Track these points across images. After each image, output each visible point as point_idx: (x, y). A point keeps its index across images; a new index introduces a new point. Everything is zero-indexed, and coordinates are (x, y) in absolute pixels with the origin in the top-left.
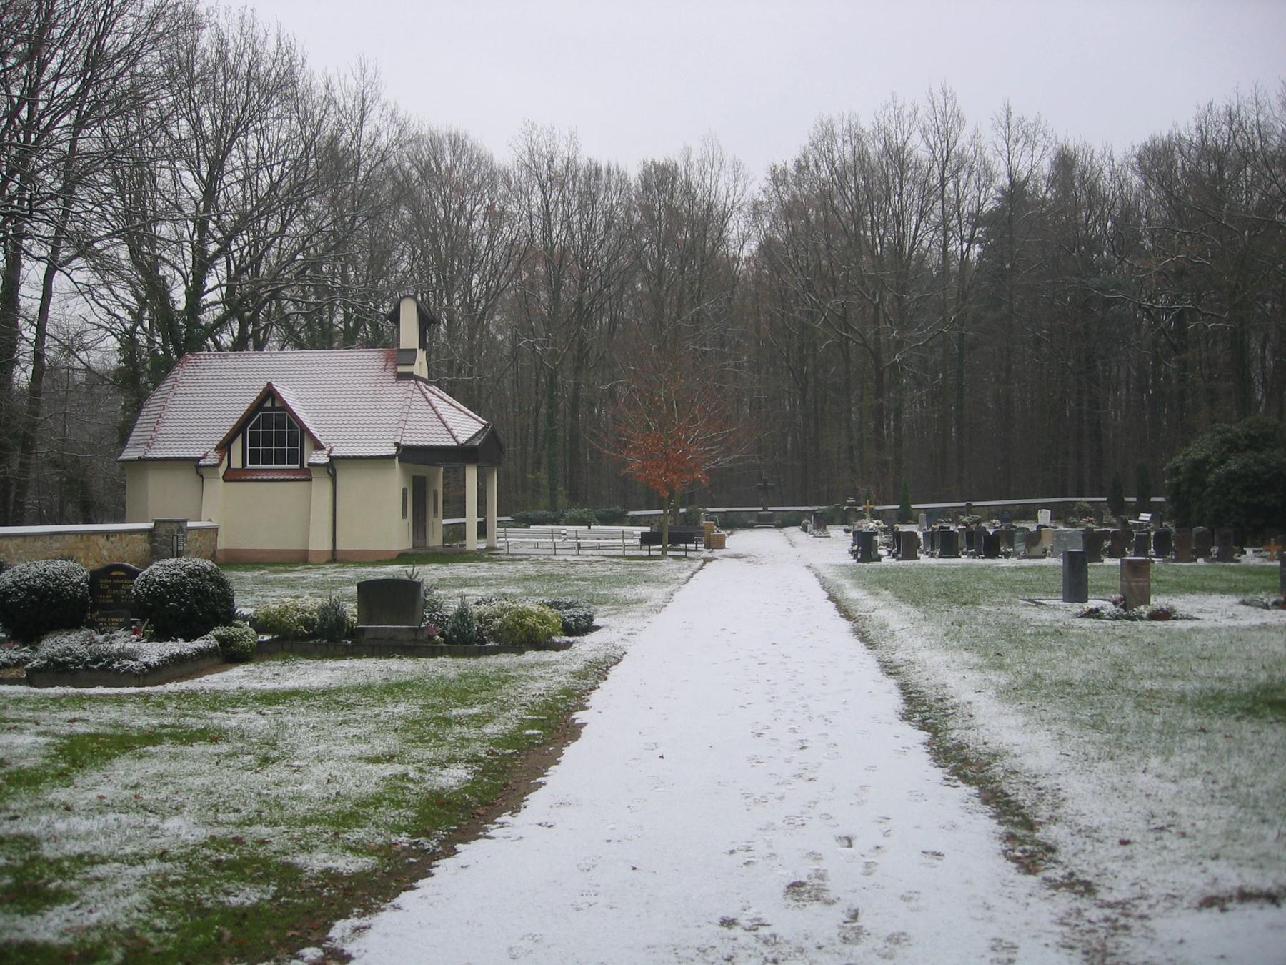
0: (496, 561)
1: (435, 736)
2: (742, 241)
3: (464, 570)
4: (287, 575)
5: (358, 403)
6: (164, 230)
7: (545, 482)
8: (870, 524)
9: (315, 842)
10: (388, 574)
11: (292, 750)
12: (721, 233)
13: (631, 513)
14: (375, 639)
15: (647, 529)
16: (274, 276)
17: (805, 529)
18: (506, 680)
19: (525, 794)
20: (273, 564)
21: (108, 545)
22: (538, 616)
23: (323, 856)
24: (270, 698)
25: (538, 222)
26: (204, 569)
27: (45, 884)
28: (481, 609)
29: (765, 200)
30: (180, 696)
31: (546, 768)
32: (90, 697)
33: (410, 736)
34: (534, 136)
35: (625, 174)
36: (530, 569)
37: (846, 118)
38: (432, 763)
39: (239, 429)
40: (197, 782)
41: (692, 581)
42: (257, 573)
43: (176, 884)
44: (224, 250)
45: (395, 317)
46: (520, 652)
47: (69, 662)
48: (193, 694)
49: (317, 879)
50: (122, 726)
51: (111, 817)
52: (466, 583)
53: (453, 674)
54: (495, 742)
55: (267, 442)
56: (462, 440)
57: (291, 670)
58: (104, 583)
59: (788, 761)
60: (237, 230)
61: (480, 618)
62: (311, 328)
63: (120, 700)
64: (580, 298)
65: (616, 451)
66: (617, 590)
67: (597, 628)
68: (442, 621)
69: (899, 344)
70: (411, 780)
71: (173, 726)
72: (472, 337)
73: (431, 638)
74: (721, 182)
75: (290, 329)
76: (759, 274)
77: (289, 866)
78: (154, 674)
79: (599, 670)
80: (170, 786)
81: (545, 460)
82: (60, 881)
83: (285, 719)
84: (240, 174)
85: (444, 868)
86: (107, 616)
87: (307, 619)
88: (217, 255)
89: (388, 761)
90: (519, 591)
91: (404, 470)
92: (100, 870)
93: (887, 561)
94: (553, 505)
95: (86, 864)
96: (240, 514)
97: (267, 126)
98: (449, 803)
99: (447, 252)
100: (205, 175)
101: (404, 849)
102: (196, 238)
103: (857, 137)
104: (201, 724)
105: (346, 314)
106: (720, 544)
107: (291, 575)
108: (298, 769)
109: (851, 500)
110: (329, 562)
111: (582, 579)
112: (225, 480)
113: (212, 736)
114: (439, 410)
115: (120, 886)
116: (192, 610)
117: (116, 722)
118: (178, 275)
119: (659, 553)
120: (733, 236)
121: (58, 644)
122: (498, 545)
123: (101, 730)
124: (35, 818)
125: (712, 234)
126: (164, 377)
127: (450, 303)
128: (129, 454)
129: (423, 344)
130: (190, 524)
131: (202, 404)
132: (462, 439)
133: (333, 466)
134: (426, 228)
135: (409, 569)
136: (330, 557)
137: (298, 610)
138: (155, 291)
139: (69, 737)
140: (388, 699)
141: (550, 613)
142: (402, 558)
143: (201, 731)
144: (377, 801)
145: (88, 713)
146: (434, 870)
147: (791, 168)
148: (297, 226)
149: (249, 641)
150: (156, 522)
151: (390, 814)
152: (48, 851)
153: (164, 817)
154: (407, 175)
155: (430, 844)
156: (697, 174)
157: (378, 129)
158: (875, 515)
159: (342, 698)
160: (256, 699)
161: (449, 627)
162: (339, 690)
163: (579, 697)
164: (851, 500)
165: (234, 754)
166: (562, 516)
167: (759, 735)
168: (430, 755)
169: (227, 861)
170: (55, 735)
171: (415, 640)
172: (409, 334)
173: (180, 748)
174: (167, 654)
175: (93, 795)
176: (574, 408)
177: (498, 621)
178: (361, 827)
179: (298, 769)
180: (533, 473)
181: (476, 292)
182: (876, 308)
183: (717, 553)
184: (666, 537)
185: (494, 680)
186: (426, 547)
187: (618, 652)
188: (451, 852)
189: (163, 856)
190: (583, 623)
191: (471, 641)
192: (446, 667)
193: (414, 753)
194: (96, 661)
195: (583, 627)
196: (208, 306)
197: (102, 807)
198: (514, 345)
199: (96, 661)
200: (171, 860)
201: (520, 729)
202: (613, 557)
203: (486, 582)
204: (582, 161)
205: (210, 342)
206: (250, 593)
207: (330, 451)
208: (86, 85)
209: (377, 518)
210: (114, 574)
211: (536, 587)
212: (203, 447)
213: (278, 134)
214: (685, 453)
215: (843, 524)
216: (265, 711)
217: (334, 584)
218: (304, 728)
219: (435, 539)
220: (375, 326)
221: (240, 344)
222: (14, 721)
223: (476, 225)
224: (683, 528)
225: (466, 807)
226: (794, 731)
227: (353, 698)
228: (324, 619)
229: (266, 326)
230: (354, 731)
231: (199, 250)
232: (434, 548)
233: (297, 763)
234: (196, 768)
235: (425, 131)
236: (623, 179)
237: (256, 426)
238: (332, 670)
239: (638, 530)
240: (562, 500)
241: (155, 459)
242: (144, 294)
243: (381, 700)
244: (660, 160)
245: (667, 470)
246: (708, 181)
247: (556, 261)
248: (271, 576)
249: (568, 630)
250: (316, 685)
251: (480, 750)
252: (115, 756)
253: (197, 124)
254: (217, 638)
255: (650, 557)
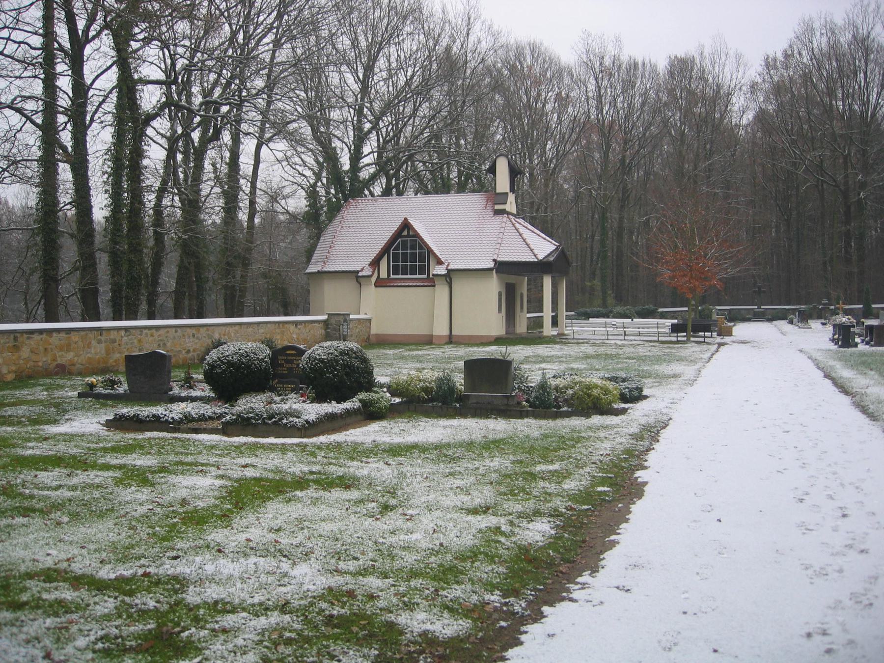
0: (565, 343)
1: (523, 490)
2: (743, 111)
3: (542, 350)
4: (417, 352)
5: (468, 231)
6: (335, 115)
7: (599, 288)
8: (844, 319)
9: (417, 599)
10: (489, 352)
11: (408, 499)
12: (727, 107)
13: (660, 310)
14: (477, 403)
15: (675, 321)
16: (409, 145)
17: (791, 322)
18: (579, 440)
19: (602, 552)
20: (408, 344)
21: (297, 331)
22: (601, 388)
23: (422, 616)
24: (395, 451)
25: (593, 103)
26: (352, 350)
27: (180, 632)
28: (558, 381)
29: (760, 81)
30: (328, 447)
31: (618, 524)
32: (263, 446)
33: (503, 489)
34: (590, 41)
35: (656, 66)
36: (590, 350)
37: (823, 16)
38: (520, 515)
39: (385, 250)
40: (327, 528)
41: (712, 360)
42: (397, 351)
43: (289, 642)
44: (375, 127)
45: (492, 170)
46: (588, 416)
47: (251, 418)
48: (338, 445)
49: (415, 643)
50: (280, 472)
51: (253, 559)
52: (544, 360)
53: (536, 434)
54: (572, 498)
55: (405, 259)
56: (541, 257)
57: (414, 427)
58: (281, 359)
59: (835, 529)
60: (383, 113)
61: (557, 388)
62: (435, 181)
63: (284, 449)
64: (624, 157)
65: (652, 265)
66: (656, 367)
67: (646, 397)
68: (528, 391)
69: (863, 185)
70: (503, 534)
71: (319, 473)
72: (546, 185)
73: (519, 403)
74: (727, 69)
75: (421, 182)
76: (754, 135)
77: (391, 625)
78: (312, 428)
79: (651, 433)
80: (306, 531)
81: (598, 272)
82: (193, 629)
83: (404, 470)
84: (384, 74)
85: (533, 633)
86: (283, 383)
87: (427, 387)
88: (370, 132)
89: (485, 512)
90: (583, 366)
91: (499, 278)
92: (229, 620)
93: (862, 347)
94: (604, 304)
95: (219, 612)
96: (386, 309)
97: (403, 40)
98: (535, 559)
99: (528, 128)
100: (361, 77)
101: (495, 608)
102: (355, 118)
103: (832, 30)
104: (340, 471)
105: (459, 170)
106: (729, 333)
107: (420, 353)
108: (411, 518)
109: (825, 301)
110: (447, 343)
111: (629, 358)
112: (376, 286)
113: (346, 483)
114: (524, 236)
115: (240, 642)
116: (342, 380)
117: (277, 468)
118: (344, 146)
119: (685, 339)
120: (735, 108)
121: (253, 403)
122: (566, 332)
123: (265, 474)
124: (191, 558)
125: (721, 104)
126: (335, 216)
127: (531, 161)
128: (312, 269)
129: (512, 190)
130: (351, 317)
131: (360, 234)
132: (541, 257)
133: (450, 276)
134: (514, 110)
135: (503, 349)
136: (447, 340)
137: (420, 381)
138: (331, 157)
139: (238, 480)
140: (486, 455)
141: (610, 385)
142: (498, 341)
143: (341, 478)
144: (473, 555)
145: (258, 460)
146: (523, 638)
147: (780, 57)
148: (425, 109)
149: (384, 403)
150: (329, 315)
151: (484, 570)
152: (192, 597)
153: (294, 564)
154: (499, 71)
155: (519, 606)
156: (708, 63)
157: (480, 40)
158: (846, 312)
159: (450, 453)
160: (384, 451)
161: (533, 395)
162: (448, 445)
163: (638, 457)
164: (825, 301)
165: (361, 501)
166: (611, 312)
167: (801, 500)
168: (519, 508)
169: (340, 616)
170: (230, 479)
171: (508, 405)
172: (503, 182)
173: (321, 493)
174: (323, 413)
175: (242, 537)
176: (620, 235)
177: (570, 392)
178: (458, 583)
179: (411, 518)
180: (590, 281)
181: (549, 154)
182: (846, 158)
183: (727, 339)
184: (690, 327)
185: (569, 439)
186: (514, 333)
187: (665, 418)
188: (538, 617)
189: (284, 607)
190: (635, 393)
191: (549, 407)
192: (529, 428)
193: (505, 506)
194: (270, 418)
195: (635, 396)
196: (364, 167)
197: (248, 550)
198: (576, 191)
199: (270, 418)
200: (291, 612)
201: (593, 486)
202: (650, 341)
203: (559, 359)
204: (624, 58)
205: (367, 192)
206: (391, 365)
207: (448, 265)
208: (280, 17)
209: (481, 312)
210: (288, 352)
211: (596, 363)
212: (361, 263)
213: (410, 45)
214: (704, 267)
215: (818, 318)
216: (390, 462)
217: (449, 360)
218: (419, 478)
219: (521, 328)
220: (479, 178)
221: (387, 192)
222: (203, 465)
223: (549, 107)
224: (700, 324)
225: (551, 564)
226: (831, 497)
227: (459, 452)
228: (439, 387)
229: (405, 180)
230: (458, 483)
231: (358, 129)
232: (520, 334)
233: (410, 512)
234: (329, 516)
235: (512, 41)
236: (654, 69)
237: (397, 248)
238: (445, 427)
239: (669, 322)
240: (610, 300)
241: (329, 272)
242: (321, 160)
243: (480, 455)
244: (681, 54)
245: (691, 277)
246: (717, 69)
247: (606, 131)
248: (407, 353)
249: (624, 399)
250: (431, 440)
251: (560, 504)
252: (270, 499)
253: (355, 43)
254: (360, 401)
255: (678, 342)
